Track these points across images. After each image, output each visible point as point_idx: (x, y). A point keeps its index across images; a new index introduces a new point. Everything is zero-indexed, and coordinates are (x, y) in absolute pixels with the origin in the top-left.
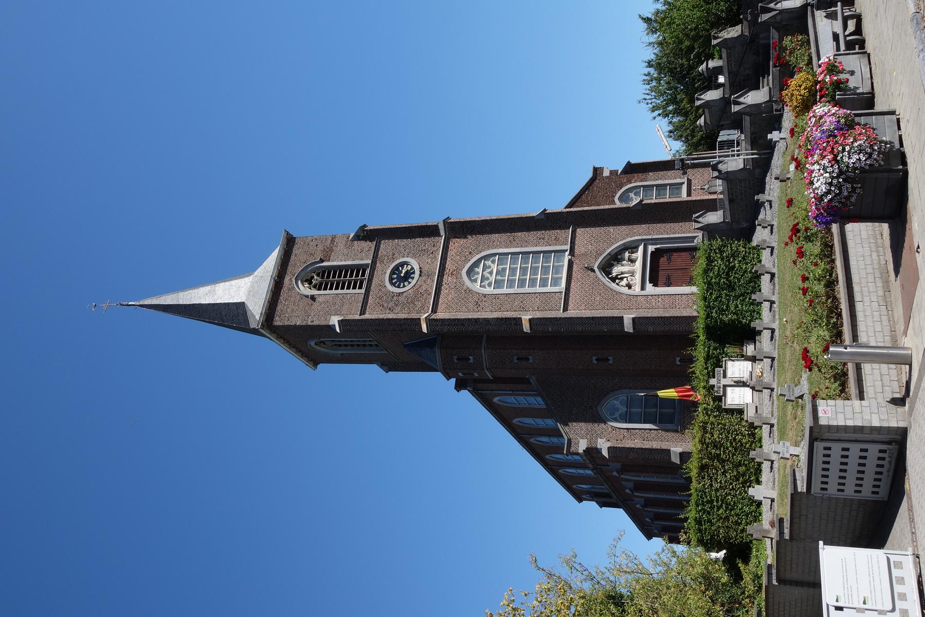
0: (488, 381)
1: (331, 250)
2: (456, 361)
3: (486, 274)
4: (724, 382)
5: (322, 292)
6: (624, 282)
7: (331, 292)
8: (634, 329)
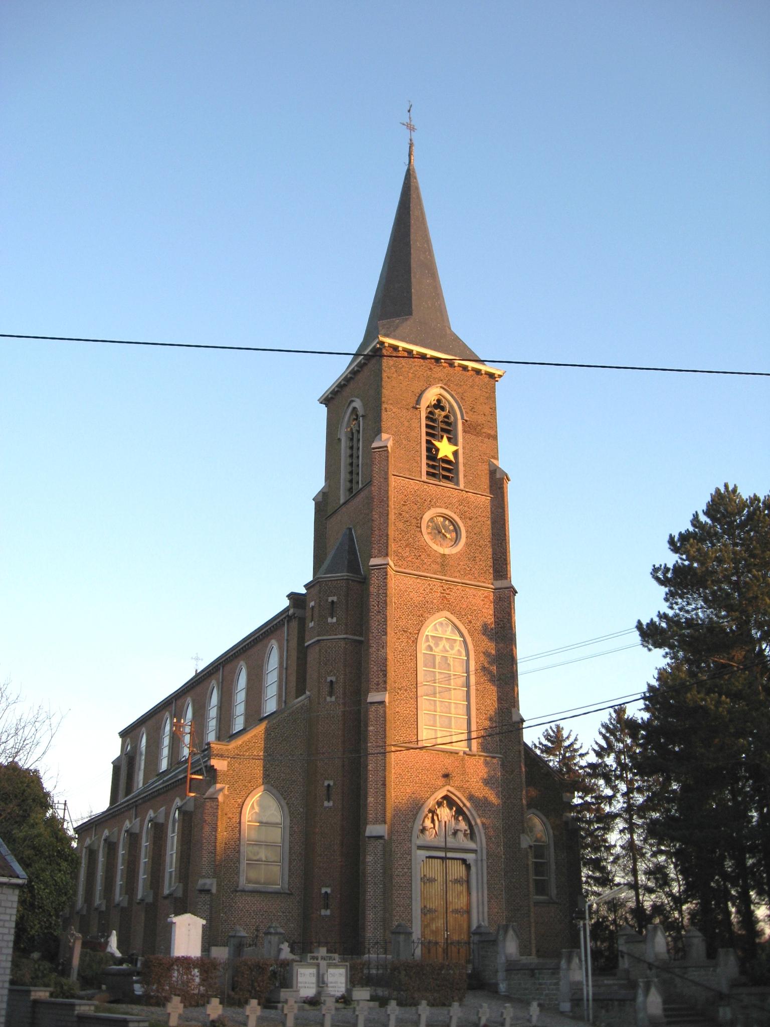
0: (301, 639)
1: (478, 434)
2: (330, 599)
3: (443, 643)
4: (323, 963)
5: (424, 422)
7: (424, 434)
8: (369, 837)
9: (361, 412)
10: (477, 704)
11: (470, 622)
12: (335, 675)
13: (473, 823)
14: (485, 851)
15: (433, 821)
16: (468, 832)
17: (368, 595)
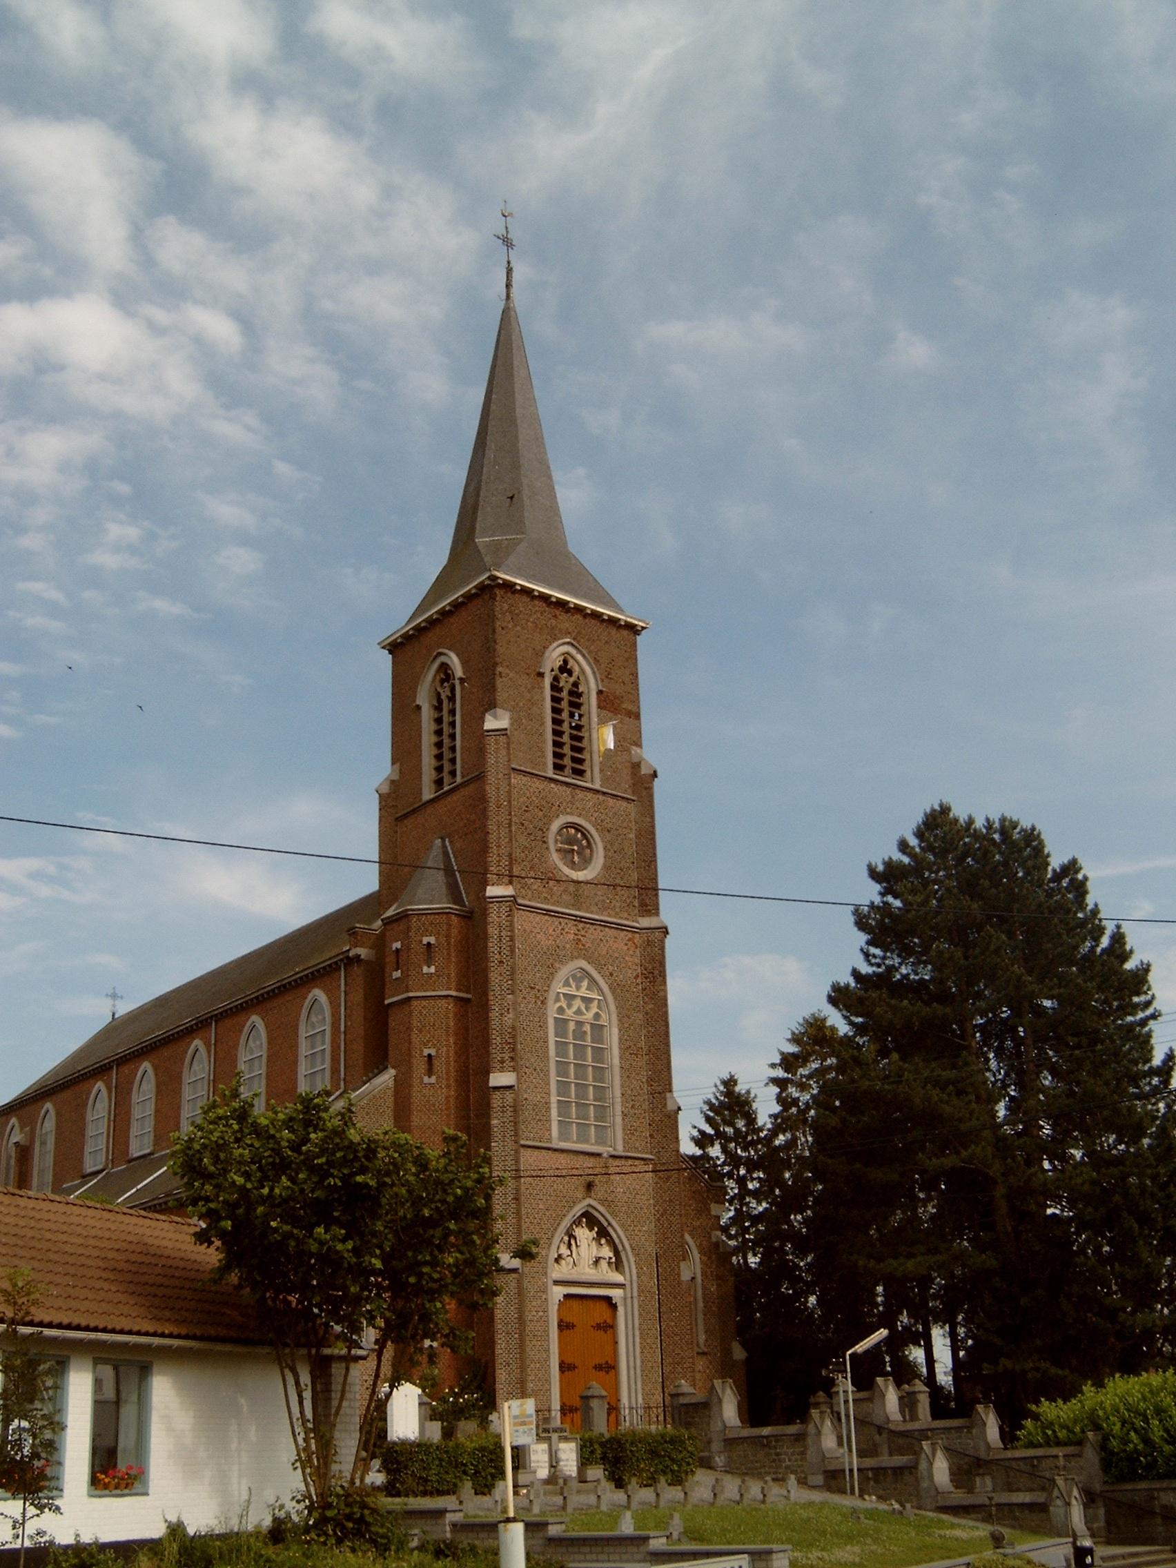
3: (577, 1003)
6: (564, 1250)
9: (459, 672)
10: (622, 1086)
11: (611, 975)
12: (434, 1046)
13: (620, 1248)
14: (635, 1285)
15: (569, 1246)
16: (613, 1260)
17: (485, 937)
